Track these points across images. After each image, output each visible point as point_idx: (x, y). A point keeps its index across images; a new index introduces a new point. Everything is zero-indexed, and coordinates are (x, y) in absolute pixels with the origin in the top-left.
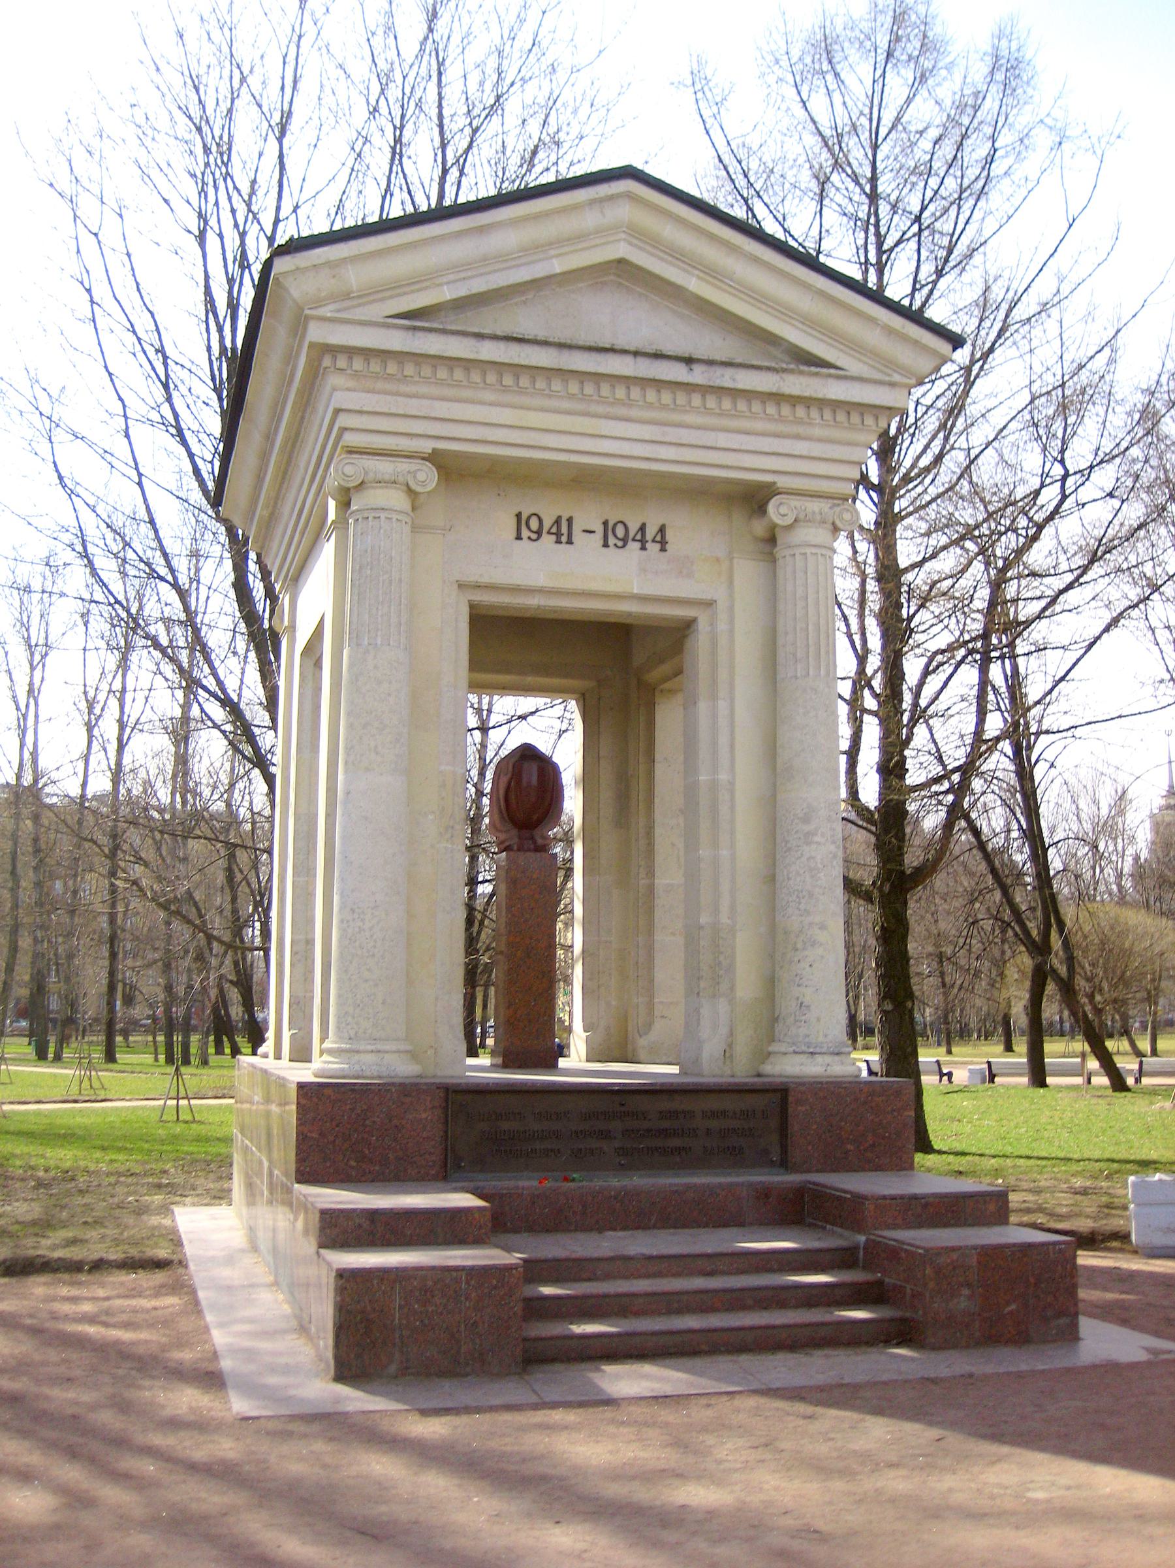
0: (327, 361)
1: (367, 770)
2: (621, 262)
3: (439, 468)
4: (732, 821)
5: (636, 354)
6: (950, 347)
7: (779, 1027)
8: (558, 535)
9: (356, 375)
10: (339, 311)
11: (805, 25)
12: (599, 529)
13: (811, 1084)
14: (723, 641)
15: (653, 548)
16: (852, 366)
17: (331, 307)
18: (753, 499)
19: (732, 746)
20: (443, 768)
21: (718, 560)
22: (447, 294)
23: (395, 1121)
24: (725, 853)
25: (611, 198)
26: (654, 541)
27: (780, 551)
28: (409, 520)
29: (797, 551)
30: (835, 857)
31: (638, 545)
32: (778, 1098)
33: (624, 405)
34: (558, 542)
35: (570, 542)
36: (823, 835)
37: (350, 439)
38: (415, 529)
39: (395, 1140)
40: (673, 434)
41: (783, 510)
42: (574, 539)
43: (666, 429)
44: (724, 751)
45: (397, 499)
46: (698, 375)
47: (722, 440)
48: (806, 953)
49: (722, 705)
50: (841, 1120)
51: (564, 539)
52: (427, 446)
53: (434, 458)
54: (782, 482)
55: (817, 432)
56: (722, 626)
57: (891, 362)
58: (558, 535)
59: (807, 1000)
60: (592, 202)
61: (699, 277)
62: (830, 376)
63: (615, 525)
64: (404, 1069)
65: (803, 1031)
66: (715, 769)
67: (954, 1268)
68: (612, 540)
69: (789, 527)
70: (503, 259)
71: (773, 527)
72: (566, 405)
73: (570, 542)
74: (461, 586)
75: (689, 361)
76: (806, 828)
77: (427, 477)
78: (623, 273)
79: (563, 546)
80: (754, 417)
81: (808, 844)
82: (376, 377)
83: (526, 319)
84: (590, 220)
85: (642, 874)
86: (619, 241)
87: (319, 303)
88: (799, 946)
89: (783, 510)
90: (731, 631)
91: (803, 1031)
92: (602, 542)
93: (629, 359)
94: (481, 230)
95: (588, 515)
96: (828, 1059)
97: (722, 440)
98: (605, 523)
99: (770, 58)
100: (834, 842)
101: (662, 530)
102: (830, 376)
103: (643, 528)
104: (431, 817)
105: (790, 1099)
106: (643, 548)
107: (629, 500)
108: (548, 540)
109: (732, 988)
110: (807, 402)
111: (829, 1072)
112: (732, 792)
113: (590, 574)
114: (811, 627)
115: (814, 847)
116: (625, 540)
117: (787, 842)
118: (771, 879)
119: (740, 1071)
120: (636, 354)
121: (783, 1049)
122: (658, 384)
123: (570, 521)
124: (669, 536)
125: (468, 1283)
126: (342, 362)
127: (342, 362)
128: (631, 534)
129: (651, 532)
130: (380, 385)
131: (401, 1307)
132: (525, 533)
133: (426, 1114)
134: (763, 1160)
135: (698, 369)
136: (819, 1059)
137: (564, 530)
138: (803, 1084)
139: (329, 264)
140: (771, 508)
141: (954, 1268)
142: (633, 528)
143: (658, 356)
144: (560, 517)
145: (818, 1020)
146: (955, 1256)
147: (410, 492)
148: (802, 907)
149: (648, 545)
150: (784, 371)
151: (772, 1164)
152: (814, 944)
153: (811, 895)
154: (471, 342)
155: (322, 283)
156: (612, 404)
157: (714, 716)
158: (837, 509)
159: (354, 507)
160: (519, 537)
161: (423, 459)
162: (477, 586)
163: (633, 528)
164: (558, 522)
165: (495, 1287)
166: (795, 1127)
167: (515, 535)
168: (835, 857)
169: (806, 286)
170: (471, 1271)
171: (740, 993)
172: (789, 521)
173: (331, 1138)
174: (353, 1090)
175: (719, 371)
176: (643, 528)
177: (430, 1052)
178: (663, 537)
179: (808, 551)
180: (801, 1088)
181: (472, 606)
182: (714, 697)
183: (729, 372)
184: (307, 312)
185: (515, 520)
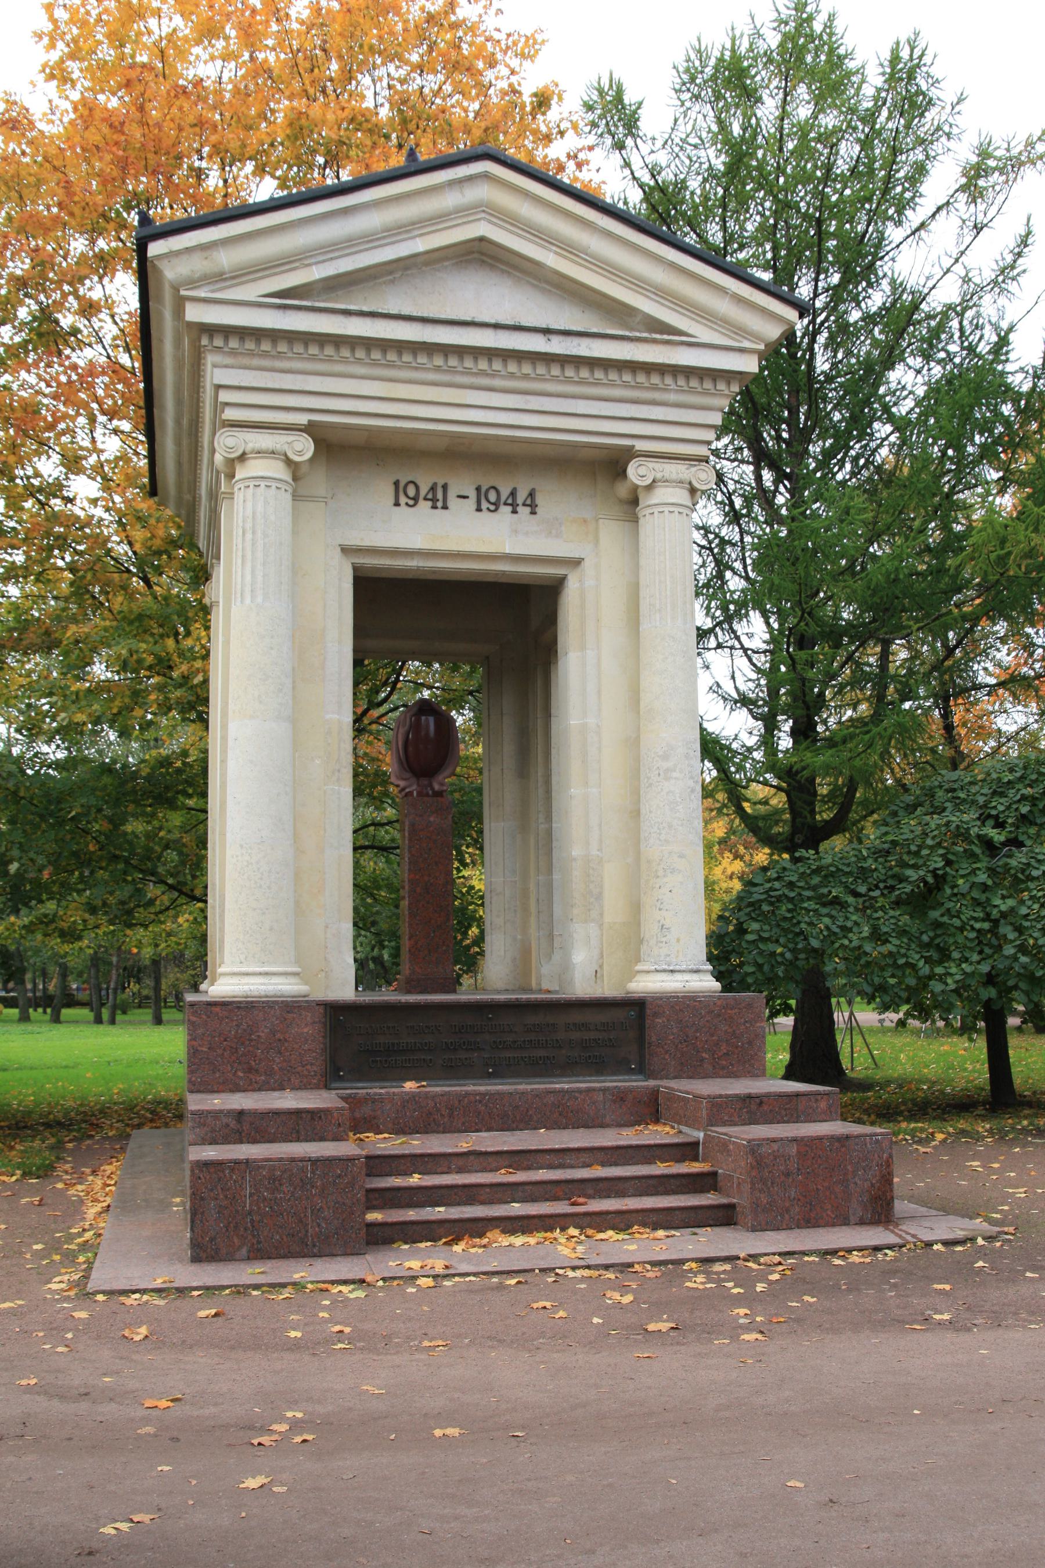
0: (205, 341)
2: (482, 239)
5: (496, 326)
6: (796, 314)
7: (644, 948)
8: (434, 500)
10: (213, 291)
11: (717, 43)
12: (473, 494)
13: (668, 998)
16: (704, 334)
19: (599, 692)
21: (585, 521)
23: (278, 1036)
25: (470, 179)
26: (524, 505)
27: (642, 511)
30: (693, 791)
31: (509, 509)
32: (636, 1009)
33: (487, 375)
34: (434, 507)
35: (445, 507)
37: (230, 414)
38: (296, 497)
41: (642, 471)
42: (450, 504)
43: (529, 397)
45: (277, 470)
46: (557, 346)
48: (666, 880)
49: (590, 654)
50: (697, 1031)
51: (440, 504)
52: (303, 419)
53: (309, 429)
54: (640, 445)
55: (672, 397)
56: (589, 582)
57: (740, 329)
58: (434, 500)
59: (667, 923)
60: (452, 183)
61: (556, 253)
62: (683, 343)
63: (487, 491)
64: (287, 987)
68: (485, 505)
69: (650, 488)
71: (635, 488)
72: (431, 376)
73: (445, 507)
74: (346, 550)
75: (547, 332)
76: (666, 765)
77: (303, 448)
78: (480, 255)
79: (439, 512)
80: (612, 385)
81: (667, 779)
82: (251, 354)
84: (451, 200)
85: (541, 819)
86: (479, 220)
87: (193, 282)
88: (661, 873)
89: (642, 471)
92: (475, 507)
94: (346, 211)
95: (462, 484)
98: (478, 489)
99: (685, 77)
100: (692, 778)
101: (532, 495)
102: (683, 343)
103: (513, 494)
104: (317, 762)
105: (648, 1012)
106: (514, 512)
107: (502, 469)
108: (424, 506)
109: (601, 915)
113: (463, 535)
115: (673, 781)
116: (497, 505)
117: (649, 778)
119: (607, 990)
120: (496, 326)
121: (646, 968)
123: (445, 487)
124: (539, 500)
125: (313, 1172)
126: (218, 342)
127: (218, 342)
128: (503, 498)
130: (256, 362)
131: (251, 1195)
132: (403, 500)
133: (309, 1031)
134: (621, 1066)
137: (440, 496)
138: (661, 998)
140: (631, 470)
142: (505, 493)
144: (435, 484)
145: (678, 940)
146: (775, 1146)
147: (288, 462)
149: (520, 509)
151: (631, 1071)
153: (670, 826)
155: (196, 265)
156: (476, 374)
159: (237, 478)
163: (505, 493)
164: (433, 489)
165: (339, 1176)
166: (652, 1036)
167: (392, 501)
168: (693, 791)
170: (315, 1162)
171: (608, 919)
173: (220, 1052)
174: (239, 1008)
175: (576, 341)
176: (513, 494)
177: (322, 975)
180: (660, 1002)
181: (356, 569)
182: (583, 648)
183: (585, 342)
184: (183, 293)
185: (393, 488)
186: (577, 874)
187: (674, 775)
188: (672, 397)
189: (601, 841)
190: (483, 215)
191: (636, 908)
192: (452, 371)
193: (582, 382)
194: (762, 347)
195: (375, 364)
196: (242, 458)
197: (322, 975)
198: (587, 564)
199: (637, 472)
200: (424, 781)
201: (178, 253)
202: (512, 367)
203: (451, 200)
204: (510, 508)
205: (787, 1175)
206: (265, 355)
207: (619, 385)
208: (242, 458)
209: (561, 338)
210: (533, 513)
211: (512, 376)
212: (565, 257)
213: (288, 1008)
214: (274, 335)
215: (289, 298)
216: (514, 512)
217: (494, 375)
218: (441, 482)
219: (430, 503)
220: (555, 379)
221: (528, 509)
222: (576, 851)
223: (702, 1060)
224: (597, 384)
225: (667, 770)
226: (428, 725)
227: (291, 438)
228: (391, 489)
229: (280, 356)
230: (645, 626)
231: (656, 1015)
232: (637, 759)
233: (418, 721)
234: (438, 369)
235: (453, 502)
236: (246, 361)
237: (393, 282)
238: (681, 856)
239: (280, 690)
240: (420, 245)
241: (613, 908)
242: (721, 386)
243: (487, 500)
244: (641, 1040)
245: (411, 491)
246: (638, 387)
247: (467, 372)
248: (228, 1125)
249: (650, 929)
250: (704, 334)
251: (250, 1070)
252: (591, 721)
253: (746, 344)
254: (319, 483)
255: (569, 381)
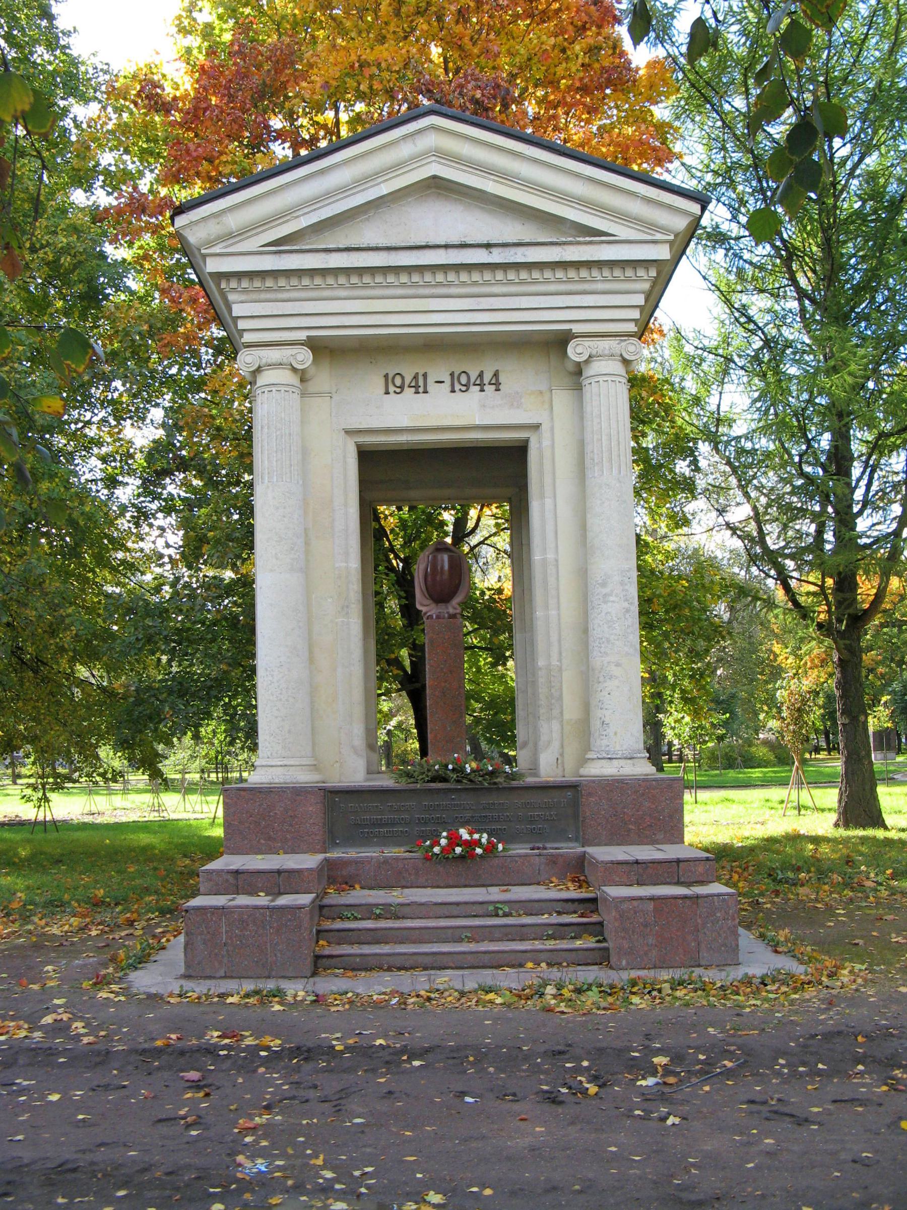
1: (271, 571)
2: (435, 177)
3: (311, 348)
4: (558, 589)
5: (446, 247)
8: (417, 387)
9: (245, 291)
10: (226, 247)
12: (448, 379)
13: (600, 781)
14: (547, 454)
15: (490, 389)
16: (622, 232)
17: (220, 246)
18: (556, 343)
20: (337, 565)
21: (541, 392)
22: (304, 222)
24: (553, 613)
25: (420, 131)
28: (297, 391)
29: (593, 380)
30: (628, 611)
34: (417, 392)
35: (425, 392)
36: (617, 596)
38: (303, 394)
39: (291, 825)
40: (485, 303)
42: (429, 389)
44: (550, 535)
46: (496, 256)
47: (525, 302)
49: (548, 502)
51: (421, 390)
52: (302, 335)
54: (576, 328)
55: (600, 286)
56: (546, 443)
58: (417, 387)
59: (607, 720)
60: (405, 137)
65: (605, 742)
66: (544, 550)
67: (635, 913)
69: (587, 362)
70: (343, 190)
74: (348, 432)
75: (488, 246)
77: (304, 357)
78: (437, 187)
80: (547, 282)
81: (605, 602)
82: (259, 290)
83: (370, 233)
84: (406, 150)
87: (211, 243)
88: (601, 679)
90: (553, 446)
91: (605, 742)
93: (442, 252)
94: (322, 172)
95: (439, 371)
96: (622, 762)
97: (525, 302)
98: (452, 375)
101: (496, 375)
103: (481, 375)
107: (466, 353)
109: (562, 713)
110: (589, 265)
111: (621, 773)
112: (557, 566)
114: (604, 438)
115: (609, 604)
116: (467, 386)
118: (585, 630)
120: (446, 247)
122: (397, 270)
123: (425, 376)
125: (271, 917)
128: (472, 380)
129: (487, 378)
130: (263, 296)
132: (392, 389)
133: (313, 809)
135: (495, 251)
136: (615, 762)
137: (421, 383)
139: (214, 215)
141: (635, 913)
143: (464, 246)
145: (616, 734)
147: (294, 370)
148: (603, 650)
149: (485, 388)
150: (565, 243)
151: (570, 840)
152: (611, 678)
153: (608, 641)
154: (323, 255)
157: (543, 512)
158: (623, 344)
159: (258, 384)
160: (387, 393)
161: (302, 344)
162: (359, 432)
163: (474, 376)
164: (416, 377)
165: (290, 920)
167: (383, 391)
169: (578, 175)
171: (567, 716)
172: (584, 357)
173: (247, 825)
175: (513, 250)
176: (481, 375)
177: (337, 765)
178: (497, 379)
179: (601, 379)
182: (542, 497)
183: (520, 250)
185: (383, 380)
186: (541, 680)
187: (611, 599)
188: (600, 286)
189: (560, 653)
190: (434, 158)
191: (586, 708)
192: (415, 285)
193: (522, 282)
194: (672, 237)
195: (354, 287)
196: (259, 370)
197: (337, 765)
198: (545, 427)
199: (576, 351)
200: (442, 606)
201: (197, 222)
202: (464, 277)
203: (406, 150)
204: (478, 388)
205: (646, 926)
206: (269, 290)
207: (555, 279)
208: (259, 370)
209: (500, 250)
210: (498, 390)
211: (464, 284)
212: (502, 183)
213: (298, 792)
214: (275, 274)
215: (281, 245)
216: (482, 390)
217: (450, 284)
218: (421, 372)
219: (413, 390)
220: (499, 282)
221: (493, 387)
222: (541, 663)
223: (629, 830)
224: (535, 282)
225: (605, 595)
226: (443, 561)
227: (294, 352)
228: (382, 381)
229: (281, 289)
230: (589, 474)
231: (590, 795)
232: (586, 585)
233: (435, 558)
234: (403, 285)
235: (431, 386)
236: (254, 296)
237: (367, 219)
238: (618, 665)
239: (292, 549)
240: (385, 189)
241: (571, 710)
242: (641, 273)
243: (459, 383)
244: (576, 816)
245: (398, 381)
246: (570, 281)
247: (428, 285)
248: (227, 880)
249: (596, 724)
250: (622, 232)
251: (270, 838)
252: (550, 556)
253: (659, 236)
254: (323, 379)
255: (511, 282)
